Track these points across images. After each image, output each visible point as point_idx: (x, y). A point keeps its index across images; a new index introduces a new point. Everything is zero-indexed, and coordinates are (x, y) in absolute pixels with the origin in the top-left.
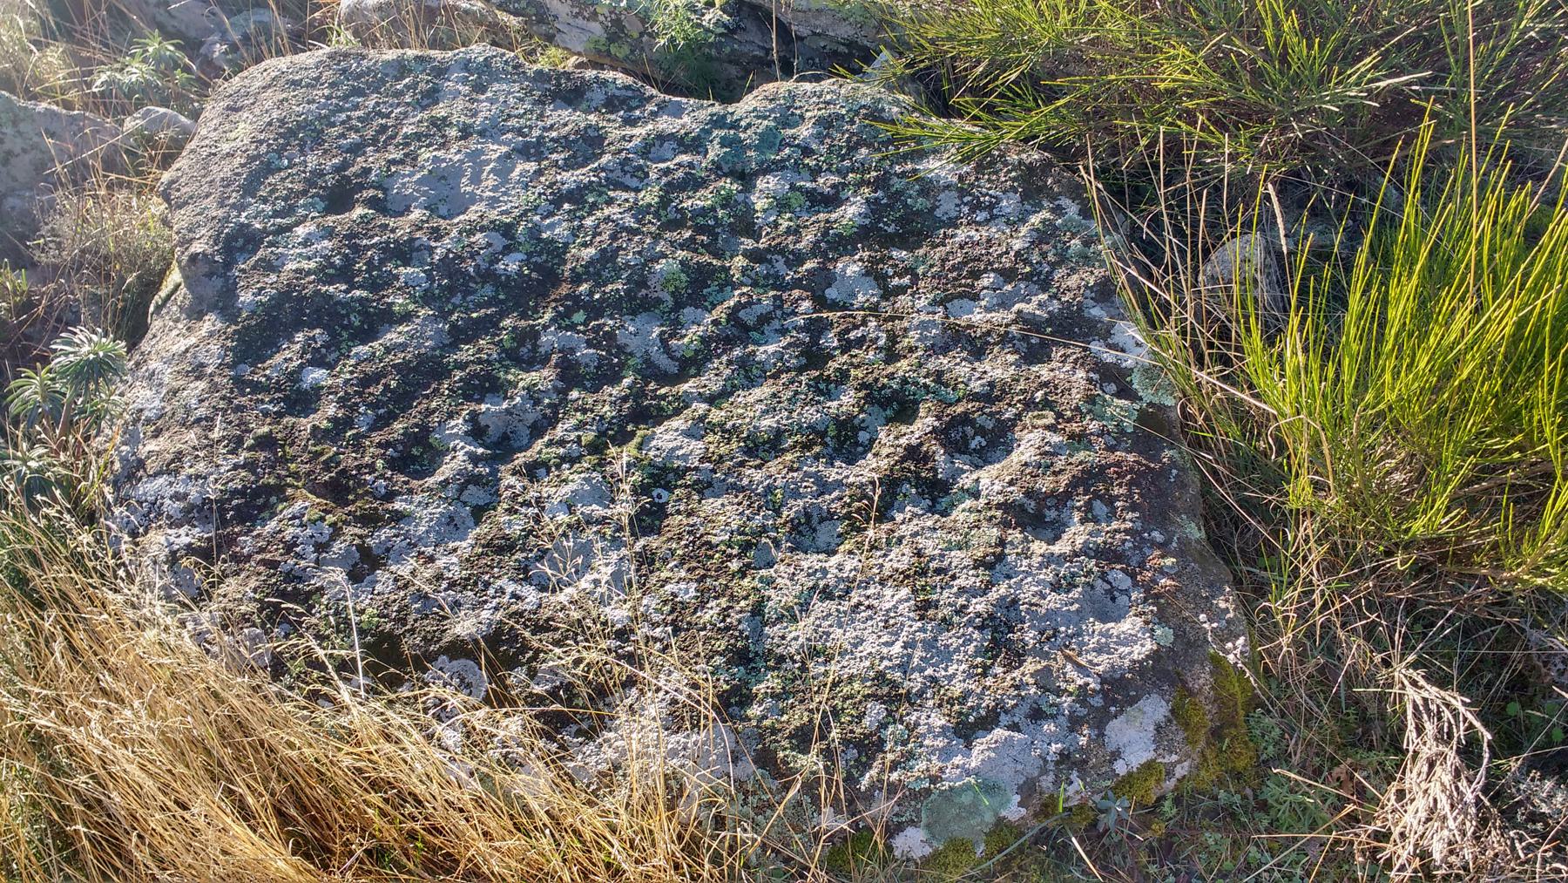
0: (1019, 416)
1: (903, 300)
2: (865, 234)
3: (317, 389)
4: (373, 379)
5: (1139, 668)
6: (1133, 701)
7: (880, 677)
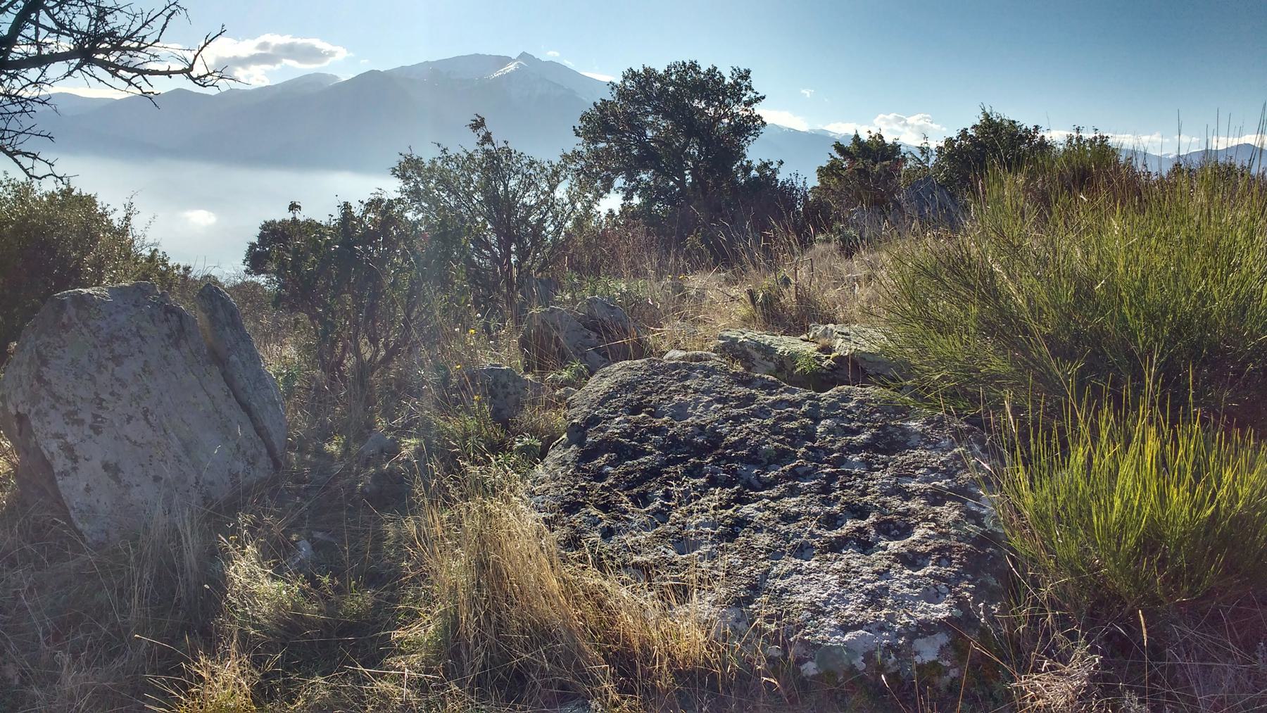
0: (918, 523)
1: (878, 474)
2: (865, 446)
3: (607, 473)
4: (632, 473)
5: (940, 622)
6: (933, 633)
7: (813, 604)
